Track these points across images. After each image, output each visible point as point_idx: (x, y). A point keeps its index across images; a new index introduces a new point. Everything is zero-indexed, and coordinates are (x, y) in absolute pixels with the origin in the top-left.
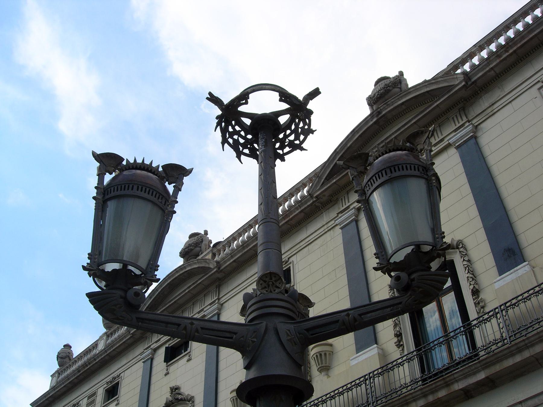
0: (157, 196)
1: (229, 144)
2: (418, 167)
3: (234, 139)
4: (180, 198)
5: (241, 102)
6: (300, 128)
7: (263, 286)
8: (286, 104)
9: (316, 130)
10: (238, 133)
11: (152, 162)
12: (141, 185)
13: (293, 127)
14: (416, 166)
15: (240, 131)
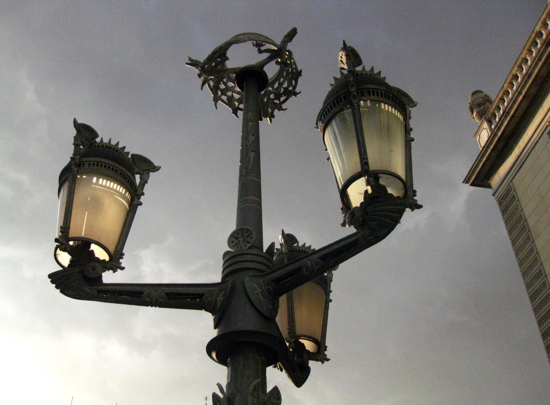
1: (223, 101)
4: (147, 189)
6: (283, 88)
7: (235, 243)
8: (392, 232)
11: (118, 143)
13: (276, 85)
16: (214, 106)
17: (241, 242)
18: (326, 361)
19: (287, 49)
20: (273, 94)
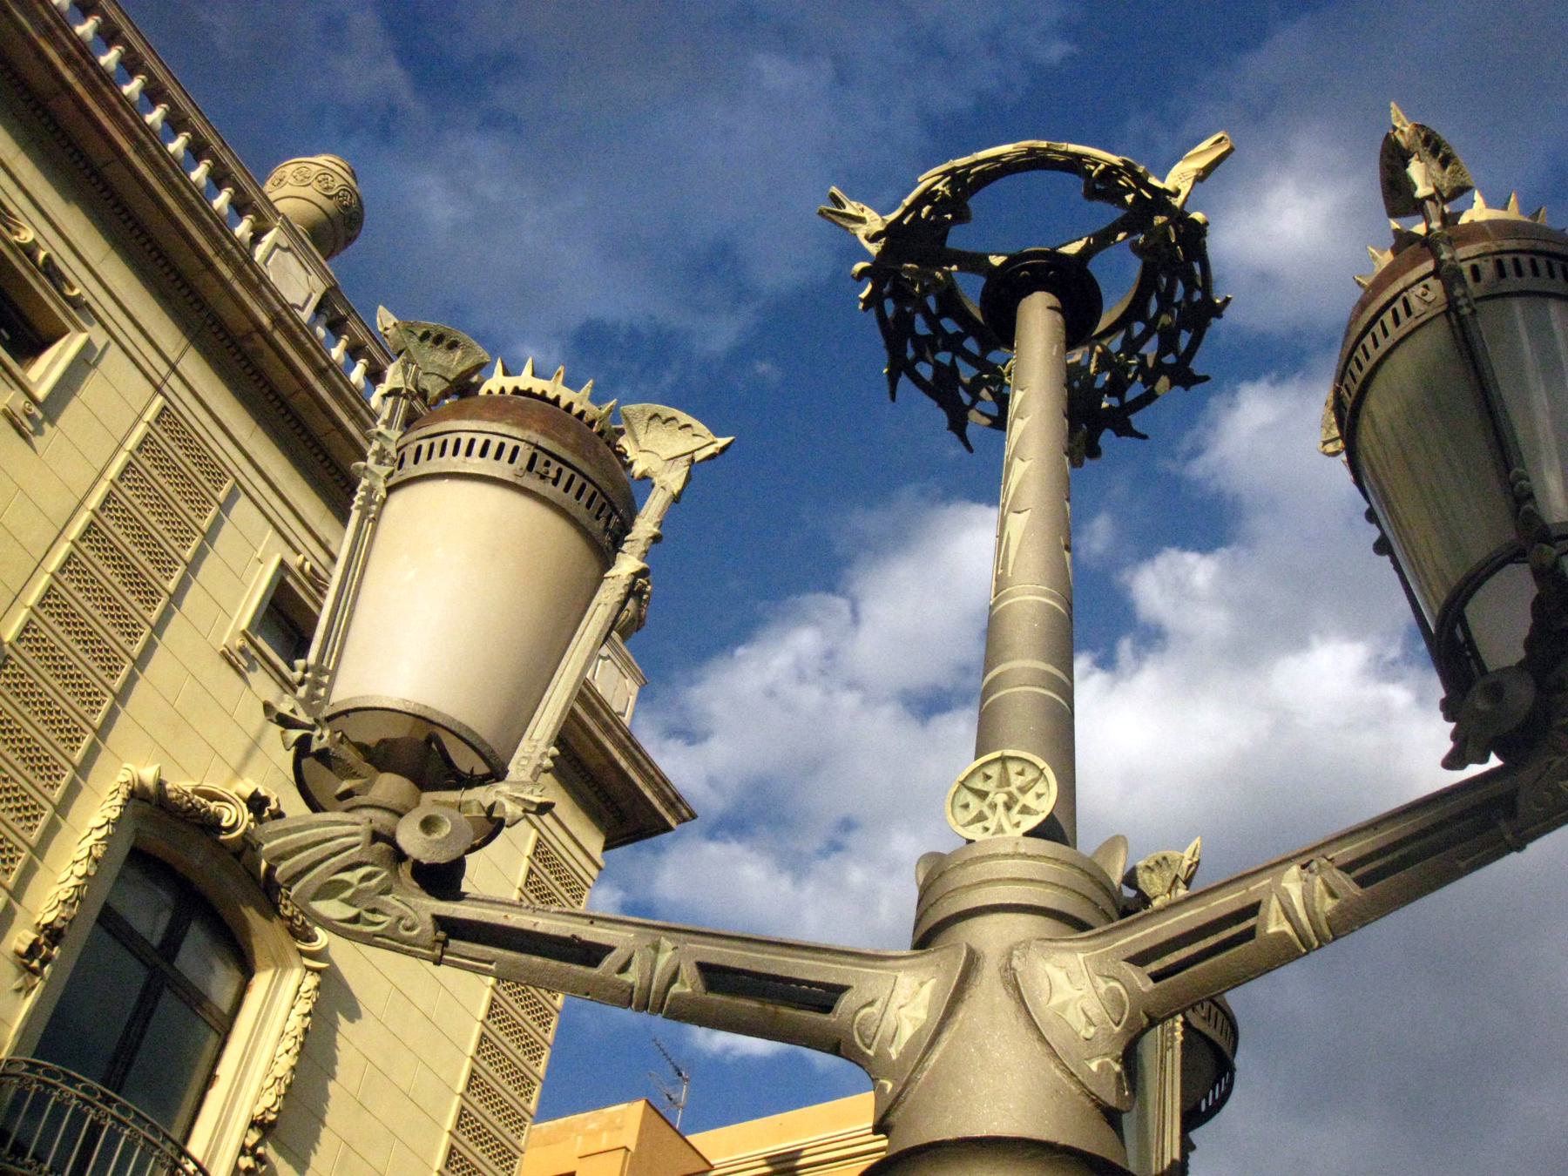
0: (596, 504)
1: (917, 379)
2: (594, 494)
3: (938, 367)
5: (1143, 191)
7: (973, 812)
9: (1206, 378)
10: (954, 344)
12: (585, 477)
14: (590, 489)
15: (959, 337)
16: (886, 389)
17: (1001, 808)
18: (1192, 337)
19: (1142, 351)
20: (101, 17)
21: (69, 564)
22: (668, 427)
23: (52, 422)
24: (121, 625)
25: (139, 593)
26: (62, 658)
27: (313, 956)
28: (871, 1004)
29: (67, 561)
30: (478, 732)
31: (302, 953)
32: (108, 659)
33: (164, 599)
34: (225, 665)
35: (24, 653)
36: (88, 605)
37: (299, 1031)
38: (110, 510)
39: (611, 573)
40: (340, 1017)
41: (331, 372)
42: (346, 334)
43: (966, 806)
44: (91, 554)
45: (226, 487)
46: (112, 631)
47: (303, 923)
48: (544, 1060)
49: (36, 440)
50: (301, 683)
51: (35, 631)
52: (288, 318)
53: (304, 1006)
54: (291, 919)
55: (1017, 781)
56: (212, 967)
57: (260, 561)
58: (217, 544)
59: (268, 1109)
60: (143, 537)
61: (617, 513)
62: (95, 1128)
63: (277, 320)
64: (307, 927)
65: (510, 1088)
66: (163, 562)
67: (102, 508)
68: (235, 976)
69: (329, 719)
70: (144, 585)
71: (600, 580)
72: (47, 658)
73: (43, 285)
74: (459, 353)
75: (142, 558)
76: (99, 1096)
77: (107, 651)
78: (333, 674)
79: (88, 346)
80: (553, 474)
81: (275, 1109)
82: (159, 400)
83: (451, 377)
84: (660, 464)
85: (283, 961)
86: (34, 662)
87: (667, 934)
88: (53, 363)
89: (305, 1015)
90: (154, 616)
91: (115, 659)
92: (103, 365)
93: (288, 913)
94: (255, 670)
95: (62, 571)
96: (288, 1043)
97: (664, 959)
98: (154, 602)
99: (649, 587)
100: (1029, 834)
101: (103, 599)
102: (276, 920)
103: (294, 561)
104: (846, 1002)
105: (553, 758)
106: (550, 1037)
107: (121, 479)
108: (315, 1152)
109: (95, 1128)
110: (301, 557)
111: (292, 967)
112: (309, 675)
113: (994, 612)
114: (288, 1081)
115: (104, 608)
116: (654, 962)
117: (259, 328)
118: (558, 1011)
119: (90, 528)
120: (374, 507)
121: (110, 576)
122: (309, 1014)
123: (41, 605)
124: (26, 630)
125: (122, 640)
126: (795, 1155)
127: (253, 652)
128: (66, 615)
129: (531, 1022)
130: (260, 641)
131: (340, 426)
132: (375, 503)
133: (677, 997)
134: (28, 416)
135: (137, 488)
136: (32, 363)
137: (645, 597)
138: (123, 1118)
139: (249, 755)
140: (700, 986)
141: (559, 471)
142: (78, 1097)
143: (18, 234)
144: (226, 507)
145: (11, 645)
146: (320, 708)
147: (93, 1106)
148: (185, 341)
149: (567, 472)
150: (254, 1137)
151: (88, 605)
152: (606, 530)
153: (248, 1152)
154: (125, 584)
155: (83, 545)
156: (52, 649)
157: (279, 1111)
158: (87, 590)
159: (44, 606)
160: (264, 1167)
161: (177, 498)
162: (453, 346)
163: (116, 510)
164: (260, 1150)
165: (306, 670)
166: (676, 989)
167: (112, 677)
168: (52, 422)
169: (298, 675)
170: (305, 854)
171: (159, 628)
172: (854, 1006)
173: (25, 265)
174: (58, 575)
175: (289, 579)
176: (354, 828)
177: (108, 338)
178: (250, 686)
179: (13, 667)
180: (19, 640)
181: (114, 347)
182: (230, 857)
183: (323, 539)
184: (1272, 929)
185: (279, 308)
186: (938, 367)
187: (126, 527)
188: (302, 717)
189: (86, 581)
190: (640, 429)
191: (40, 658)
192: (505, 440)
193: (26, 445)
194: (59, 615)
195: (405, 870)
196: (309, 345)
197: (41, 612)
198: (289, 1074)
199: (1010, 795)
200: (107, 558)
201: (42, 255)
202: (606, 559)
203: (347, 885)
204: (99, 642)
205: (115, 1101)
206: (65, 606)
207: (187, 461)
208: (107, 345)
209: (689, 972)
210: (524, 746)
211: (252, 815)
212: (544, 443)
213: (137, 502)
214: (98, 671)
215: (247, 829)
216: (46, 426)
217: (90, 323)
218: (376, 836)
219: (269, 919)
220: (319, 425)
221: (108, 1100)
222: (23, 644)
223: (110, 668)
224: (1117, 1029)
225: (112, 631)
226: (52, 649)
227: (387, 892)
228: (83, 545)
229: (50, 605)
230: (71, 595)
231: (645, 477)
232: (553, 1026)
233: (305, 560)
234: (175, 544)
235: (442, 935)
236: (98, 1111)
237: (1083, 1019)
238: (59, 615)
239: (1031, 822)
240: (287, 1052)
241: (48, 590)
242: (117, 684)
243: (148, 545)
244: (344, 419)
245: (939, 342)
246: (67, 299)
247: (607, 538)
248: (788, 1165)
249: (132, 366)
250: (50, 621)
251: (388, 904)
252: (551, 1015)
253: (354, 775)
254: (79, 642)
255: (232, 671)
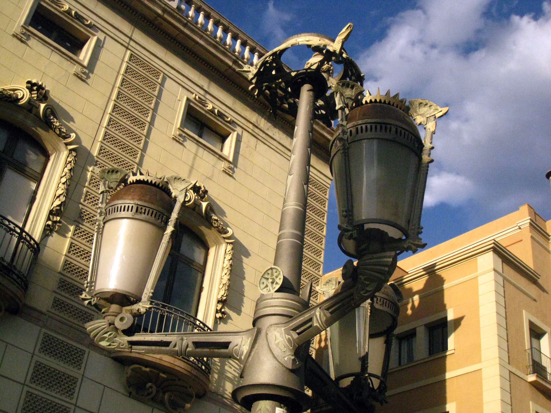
3: (289, 104)
21: (111, 122)
22: (179, 181)
23: (92, 73)
24: (134, 139)
25: (138, 125)
26: (116, 156)
27: (229, 238)
28: (237, 345)
29: (110, 121)
30: (131, 292)
31: (224, 238)
32: (132, 152)
33: (147, 125)
34: (175, 142)
35: (102, 158)
36: (120, 135)
37: (228, 266)
38: (120, 98)
39: (166, 233)
40: (243, 257)
41: (189, 24)
42: (193, 4)
43: (263, 283)
44: (117, 116)
45: (161, 77)
46: (131, 141)
47: (222, 227)
48: (322, 255)
49: (88, 81)
50: (87, 287)
51: (104, 149)
52: (168, 9)
53: (229, 257)
54: (217, 227)
55: (275, 274)
56: (193, 249)
57: (179, 100)
58: (162, 99)
59: (223, 296)
60: (135, 105)
61: (165, 215)
62: (162, 317)
63: (164, 11)
64: (224, 229)
65: (311, 268)
66: (144, 111)
67: (118, 98)
68: (203, 251)
69: (95, 295)
70: (139, 121)
71: (163, 235)
72: (111, 158)
73: (76, 23)
74: (119, 173)
75: (136, 112)
76: (161, 306)
77: (131, 149)
78: (95, 282)
79: (98, 40)
80: (143, 211)
81: (225, 295)
82: (129, 52)
83: (118, 181)
84: (178, 193)
85: (218, 242)
86: (106, 161)
87: (185, 335)
88: (87, 53)
89: (230, 260)
90: (145, 132)
91: (135, 151)
92: (105, 46)
93: (216, 225)
94: (186, 141)
95: (108, 125)
96: (225, 271)
97: (184, 342)
98: (144, 127)
99: (332, 67)
100: (276, 291)
101: (125, 131)
102: (213, 228)
103: (192, 97)
104: (231, 346)
105: (152, 293)
106: (323, 246)
107: (122, 86)
108: (243, 306)
109: (162, 317)
110: (194, 95)
111: (222, 244)
112: (88, 285)
113: (284, 209)
114: (228, 284)
115: (126, 134)
116: (182, 343)
117: (159, 15)
118: (325, 237)
119: (115, 107)
120: (101, 230)
121: (126, 122)
122: (231, 259)
123: (104, 139)
124: (101, 150)
125: (135, 144)
126: (434, 266)
127: (184, 134)
128: (114, 141)
129: (315, 243)
130: (186, 130)
131: (197, 43)
132: (101, 228)
133: (189, 351)
134: (83, 73)
135: (128, 87)
136: (80, 52)
137: (331, 72)
138: (171, 311)
139: (190, 172)
140: (194, 348)
141: (145, 210)
142: (154, 308)
143: (63, 7)
144: (162, 84)
145: (97, 157)
146: (93, 292)
147: (159, 309)
148: (133, 27)
149: (147, 209)
150: (220, 306)
151: (120, 135)
152: (162, 221)
153: (219, 312)
154: (132, 123)
155: (114, 114)
156: (112, 154)
157: (227, 295)
158: (119, 129)
159: (105, 139)
160: (226, 316)
161: (144, 86)
162: (117, 172)
163: (123, 98)
164: (223, 310)
165: (87, 283)
166: (188, 349)
167: (135, 158)
168: (92, 73)
169: (85, 285)
170: (95, 331)
171: (148, 136)
172: (232, 347)
173: (69, 18)
174: (107, 127)
175: (192, 104)
176: (105, 323)
177: (105, 35)
178: (186, 147)
179: (99, 164)
180: (99, 154)
181: (108, 37)
182: (192, 211)
183: (201, 86)
184: (315, 325)
185: (163, 6)
186: (289, 104)
187: (128, 103)
188: (88, 297)
189: (118, 126)
190: (172, 182)
191: (108, 158)
192: (129, 205)
193: (85, 84)
194: (111, 141)
195: (119, 332)
196: (178, 16)
197: (105, 142)
198: (228, 282)
199: (273, 279)
200: (123, 116)
201: (73, 12)
202: (164, 229)
203: (106, 337)
204: (127, 147)
205: (167, 306)
206: (112, 138)
207: (144, 72)
208: (105, 37)
209: (191, 345)
210: (145, 291)
211: (195, 194)
212: (139, 203)
213: (129, 92)
214: (129, 157)
215: (195, 199)
216: (90, 74)
217: (97, 32)
218: (110, 324)
219: (210, 229)
220: (190, 44)
221: (164, 306)
222: (101, 155)
223: (134, 155)
224: (291, 348)
225: (131, 141)
226: (112, 154)
227: (116, 337)
228: (114, 114)
229: (107, 139)
230: (114, 133)
231: (175, 197)
232: (323, 242)
233: (196, 95)
234: (146, 103)
235: (130, 346)
236: (161, 311)
237: (283, 346)
238: (111, 141)
239: (277, 287)
240: (226, 274)
241: (105, 133)
242: (137, 160)
243: (137, 107)
244: (198, 39)
245: (288, 96)
246: (86, 25)
247: (163, 223)
248: (432, 269)
249: (116, 42)
250: (108, 144)
251: (116, 340)
252: (322, 238)
253: (105, 307)
254: (120, 149)
255: (178, 144)
